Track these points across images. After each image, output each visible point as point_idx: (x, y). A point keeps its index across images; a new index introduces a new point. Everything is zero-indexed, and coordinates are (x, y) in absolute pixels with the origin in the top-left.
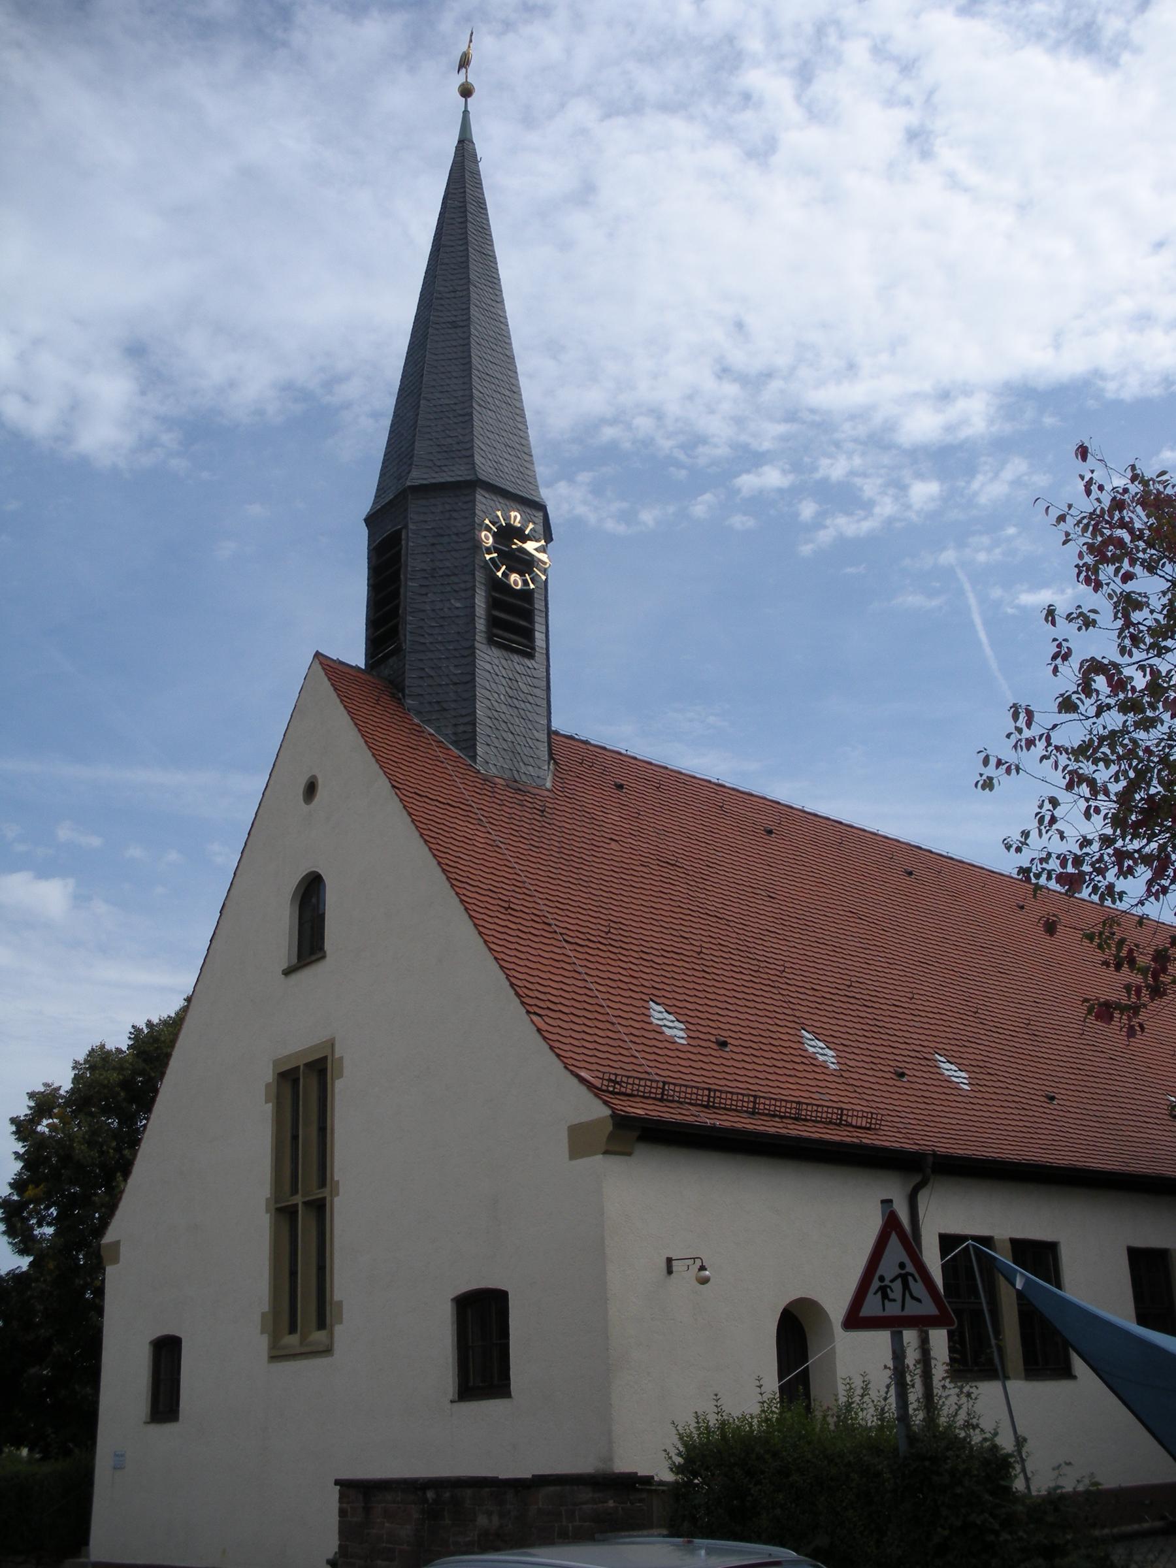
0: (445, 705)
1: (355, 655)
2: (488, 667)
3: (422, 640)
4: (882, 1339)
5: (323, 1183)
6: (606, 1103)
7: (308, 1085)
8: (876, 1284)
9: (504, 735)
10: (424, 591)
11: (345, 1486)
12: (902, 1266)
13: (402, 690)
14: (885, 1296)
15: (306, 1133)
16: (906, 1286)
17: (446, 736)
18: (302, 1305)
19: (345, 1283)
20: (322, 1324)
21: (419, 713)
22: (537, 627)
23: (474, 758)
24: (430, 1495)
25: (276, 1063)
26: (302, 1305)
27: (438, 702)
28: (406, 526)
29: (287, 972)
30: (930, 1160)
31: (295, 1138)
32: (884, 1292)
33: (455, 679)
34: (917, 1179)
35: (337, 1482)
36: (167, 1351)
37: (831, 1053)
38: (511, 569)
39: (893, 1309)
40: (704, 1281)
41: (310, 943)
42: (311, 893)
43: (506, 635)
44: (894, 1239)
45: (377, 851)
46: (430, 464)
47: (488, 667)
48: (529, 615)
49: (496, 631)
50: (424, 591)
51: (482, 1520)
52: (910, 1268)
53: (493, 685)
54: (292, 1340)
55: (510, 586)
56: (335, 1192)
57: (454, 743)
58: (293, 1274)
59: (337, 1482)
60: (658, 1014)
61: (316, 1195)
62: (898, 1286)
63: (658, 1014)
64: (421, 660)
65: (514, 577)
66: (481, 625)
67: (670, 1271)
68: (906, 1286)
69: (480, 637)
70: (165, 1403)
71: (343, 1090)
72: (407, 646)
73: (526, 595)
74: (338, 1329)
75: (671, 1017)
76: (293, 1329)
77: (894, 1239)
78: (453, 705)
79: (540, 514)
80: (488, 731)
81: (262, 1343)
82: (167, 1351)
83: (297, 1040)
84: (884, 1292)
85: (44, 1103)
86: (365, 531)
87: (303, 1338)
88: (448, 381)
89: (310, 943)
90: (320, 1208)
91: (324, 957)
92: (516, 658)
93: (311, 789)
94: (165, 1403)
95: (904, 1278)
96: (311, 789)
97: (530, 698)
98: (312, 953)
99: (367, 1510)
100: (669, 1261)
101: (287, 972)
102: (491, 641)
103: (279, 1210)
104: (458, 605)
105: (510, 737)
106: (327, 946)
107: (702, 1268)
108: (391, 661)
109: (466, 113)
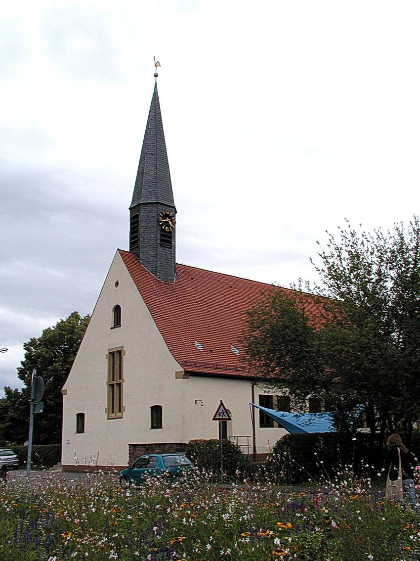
1: (127, 248)
4: (218, 421)
5: (120, 379)
6: (183, 368)
7: (117, 356)
8: (218, 413)
11: (130, 445)
13: (139, 257)
14: (220, 415)
15: (117, 367)
16: (223, 414)
17: (149, 270)
18: (115, 406)
20: (120, 411)
21: (143, 264)
22: (173, 240)
26: (115, 406)
28: (140, 213)
31: (113, 368)
32: (219, 414)
33: (152, 256)
34: (254, 382)
35: (128, 444)
36: (81, 417)
37: (238, 351)
39: (221, 417)
41: (117, 322)
42: (117, 309)
45: (132, 300)
48: (170, 237)
50: (144, 232)
57: (152, 272)
58: (113, 400)
60: (197, 344)
61: (120, 381)
62: (222, 414)
63: (197, 344)
68: (223, 414)
70: (80, 429)
73: (170, 232)
75: (200, 344)
76: (113, 412)
77: (222, 406)
79: (173, 209)
82: (81, 417)
83: (114, 346)
84: (219, 414)
85: (33, 343)
87: (115, 414)
89: (117, 322)
90: (119, 385)
93: (117, 284)
94: (80, 429)
95: (223, 413)
96: (117, 284)
98: (117, 324)
99: (135, 449)
101: (111, 328)
108: (136, 249)
109: (156, 83)
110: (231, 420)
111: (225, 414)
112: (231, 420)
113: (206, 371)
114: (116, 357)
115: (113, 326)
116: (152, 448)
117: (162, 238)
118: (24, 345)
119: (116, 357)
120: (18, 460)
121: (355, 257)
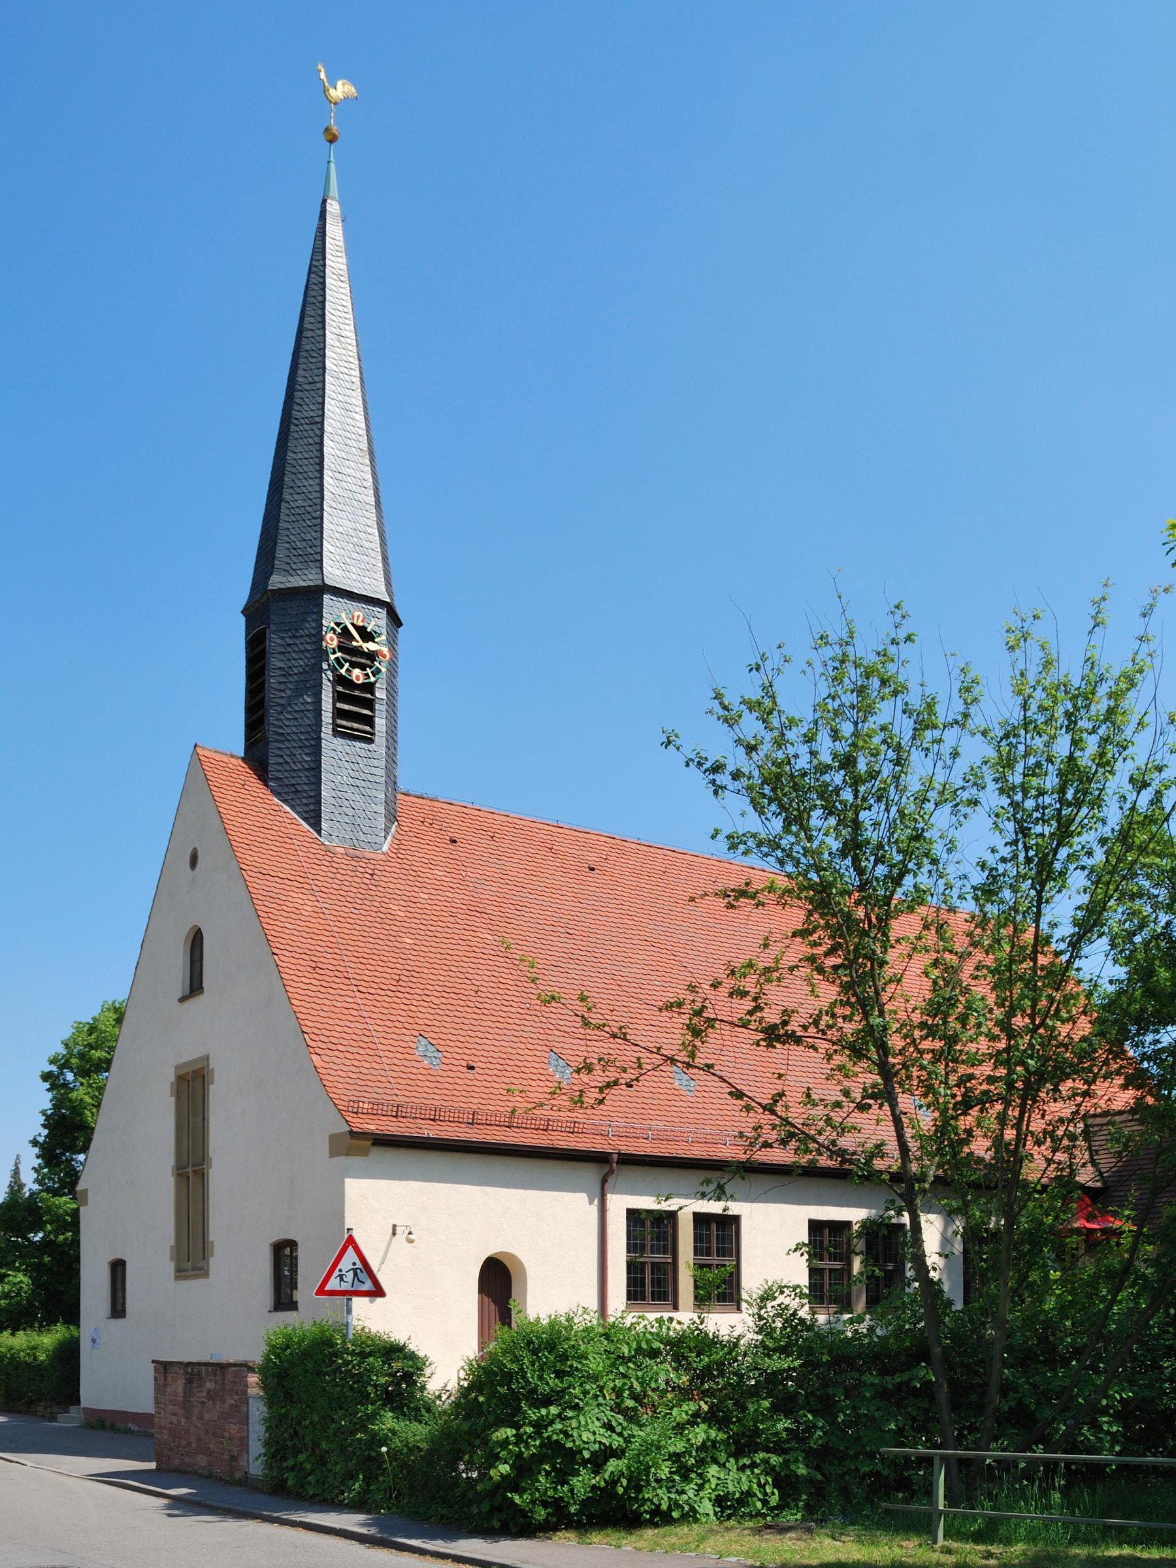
0: (299, 788)
2: (333, 754)
3: (281, 731)
8: (337, 1273)
9: (346, 810)
10: (282, 687)
12: (354, 1264)
14: (342, 1279)
18: (192, 1254)
19: (215, 1233)
23: (319, 832)
24: (189, 1370)
25: (177, 1068)
26: (192, 1254)
27: (293, 785)
29: (182, 1000)
30: (615, 1157)
32: (341, 1277)
36: (118, 1268)
38: (354, 665)
39: (345, 1286)
40: (411, 1241)
42: (196, 941)
43: (349, 724)
44: (350, 1249)
46: (288, 568)
47: (333, 754)
49: (340, 722)
50: (282, 687)
51: (208, 1385)
52: (359, 1265)
53: (338, 770)
54: (189, 1265)
55: (352, 681)
56: (209, 1166)
59: (153, 1362)
62: (351, 1275)
64: (280, 748)
65: (357, 672)
66: (327, 717)
67: (394, 1234)
68: (355, 1274)
69: (326, 730)
70: (118, 1309)
71: (215, 1091)
72: (271, 736)
74: (212, 1260)
77: (350, 1249)
78: (306, 788)
80: (332, 809)
81: (170, 1267)
82: (118, 1268)
83: (189, 1054)
84: (341, 1277)
86: (242, 620)
88: (305, 483)
89: (195, 986)
91: (202, 992)
92: (358, 744)
94: (118, 1309)
97: (370, 778)
100: (394, 1227)
101: (182, 1000)
102: (336, 733)
103: (179, 1175)
104: (309, 700)
105: (350, 812)
106: (204, 985)
107: (410, 1233)
110: (377, 1292)
111: (363, 1276)
112: (377, 1292)
113: (430, 1131)
114: (192, 1086)
115: (188, 992)
116: (199, 1374)
117: (339, 705)
118: (979, 868)
119: (192, 1086)
120: (152, 1465)
121: (866, 681)
